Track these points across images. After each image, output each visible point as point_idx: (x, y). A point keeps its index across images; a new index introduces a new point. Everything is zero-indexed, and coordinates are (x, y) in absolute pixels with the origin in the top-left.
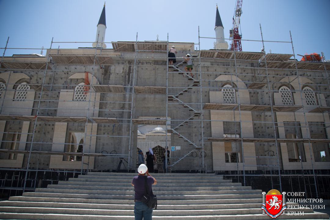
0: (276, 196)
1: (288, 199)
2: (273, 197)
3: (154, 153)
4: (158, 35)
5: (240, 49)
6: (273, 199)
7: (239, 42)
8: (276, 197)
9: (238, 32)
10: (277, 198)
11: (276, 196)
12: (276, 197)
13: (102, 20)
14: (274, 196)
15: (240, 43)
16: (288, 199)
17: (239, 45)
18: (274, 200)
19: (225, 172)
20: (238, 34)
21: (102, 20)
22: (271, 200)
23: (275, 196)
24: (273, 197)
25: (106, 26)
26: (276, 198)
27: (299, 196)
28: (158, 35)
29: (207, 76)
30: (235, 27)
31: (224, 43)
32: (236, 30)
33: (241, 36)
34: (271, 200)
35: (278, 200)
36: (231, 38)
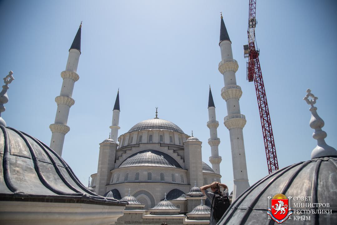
0: (282, 200)
1: (294, 204)
2: (279, 202)
3: (185, 198)
4: (310, 94)
5: (258, 68)
6: (279, 204)
7: (256, 59)
8: (282, 202)
9: (254, 47)
10: (283, 202)
11: (282, 200)
12: (282, 202)
13: (76, 45)
14: (279, 200)
15: (258, 60)
16: (294, 204)
17: (257, 63)
18: (280, 204)
19: (236, 186)
20: (255, 50)
21: (76, 45)
22: (277, 205)
23: (280, 201)
24: (279, 202)
25: (215, 107)
26: (282, 203)
27: (306, 200)
28: (310, 94)
29: (235, 105)
30: (250, 42)
31: (231, 62)
32: (252, 45)
33: (259, 51)
34: (277, 205)
35: (284, 204)
36: (246, 55)
